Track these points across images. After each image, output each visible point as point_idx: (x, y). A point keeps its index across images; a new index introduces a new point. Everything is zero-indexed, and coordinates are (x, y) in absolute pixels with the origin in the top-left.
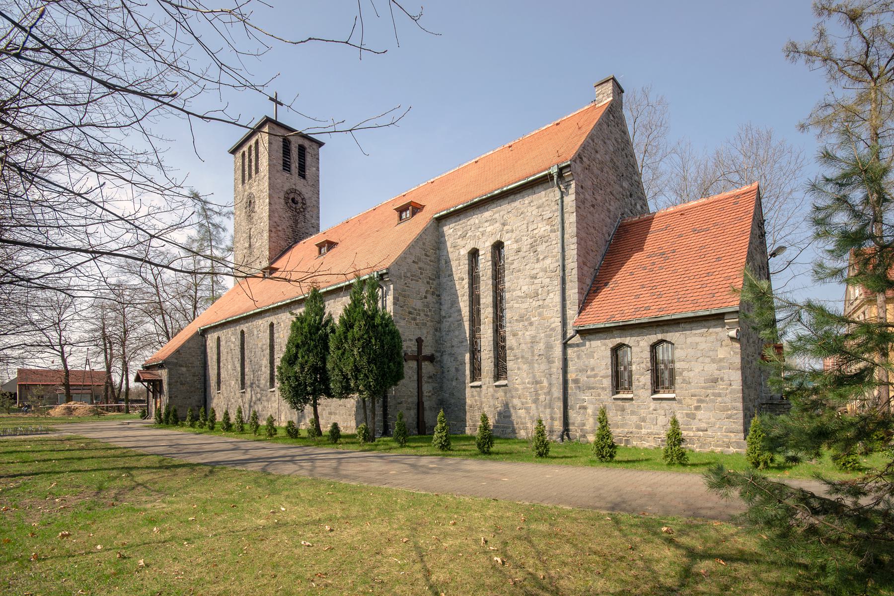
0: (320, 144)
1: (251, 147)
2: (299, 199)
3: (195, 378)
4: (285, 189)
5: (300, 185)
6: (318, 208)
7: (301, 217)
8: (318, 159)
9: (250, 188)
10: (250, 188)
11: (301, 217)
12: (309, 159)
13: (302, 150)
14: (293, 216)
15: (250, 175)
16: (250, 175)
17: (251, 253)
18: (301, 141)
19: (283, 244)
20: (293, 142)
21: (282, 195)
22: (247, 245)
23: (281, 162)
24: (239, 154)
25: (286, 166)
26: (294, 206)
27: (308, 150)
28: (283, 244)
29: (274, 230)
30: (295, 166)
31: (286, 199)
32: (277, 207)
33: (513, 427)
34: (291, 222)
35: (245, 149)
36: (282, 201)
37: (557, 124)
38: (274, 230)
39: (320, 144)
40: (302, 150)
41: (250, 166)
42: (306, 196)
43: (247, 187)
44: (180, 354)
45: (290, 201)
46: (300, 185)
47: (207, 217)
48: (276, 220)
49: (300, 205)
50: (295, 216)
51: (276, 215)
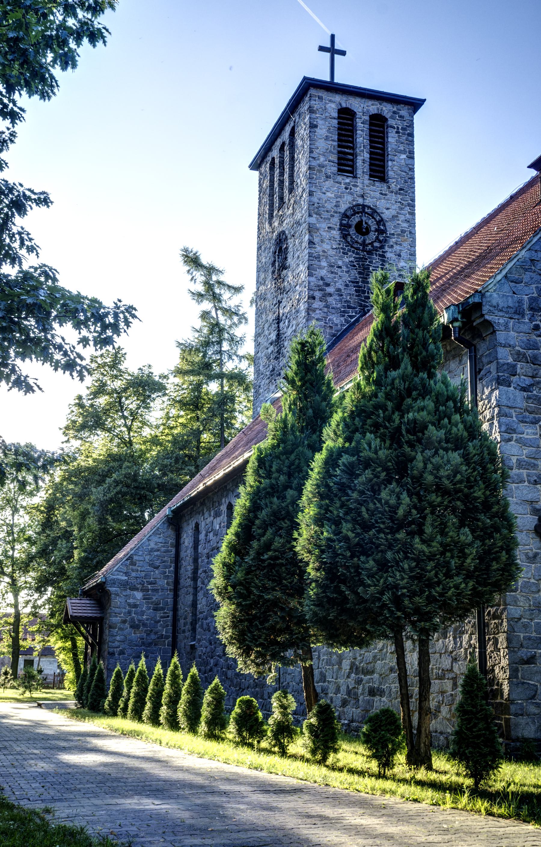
0: (415, 104)
1: (283, 144)
2: (372, 224)
3: (159, 614)
4: (343, 208)
5: (374, 195)
6: (412, 234)
7: (376, 259)
8: (411, 135)
9: (281, 223)
10: (281, 223)
11: (376, 259)
12: (392, 138)
13: (378, 123)
14: (359, 259)
15: (281, 199)
16: (281, 199)
17: (279, 352)
18: (373, 107)
19: (337, 320)
20: (359, 114)
21: (336, 221)
22: (273, 337)
23: (334, 158)
24: (266, 168)
25: (346, 165)
26: (360, 239)
27: (391, 122)
28: (337, 320)
29: (318, 294)
30: (363, 157)
31: (344, 228)
32: (326, 247)
33: (511, 558)
34: (354, 273)
35: (275, 153)
36: (336, 233)
37: (416, 801)
38: (318, 294)
39: (415, 104)
40: (378, 123)
41: (281, 182)
42: (387, 215)
43: (276, 224)
44: (133, 564)
45: (352, 231)
46: (374, 195)
47: (216, 298)
48: (323, 272)
49: (372, 236)
50: (364, 259)
51: (324, 263)
